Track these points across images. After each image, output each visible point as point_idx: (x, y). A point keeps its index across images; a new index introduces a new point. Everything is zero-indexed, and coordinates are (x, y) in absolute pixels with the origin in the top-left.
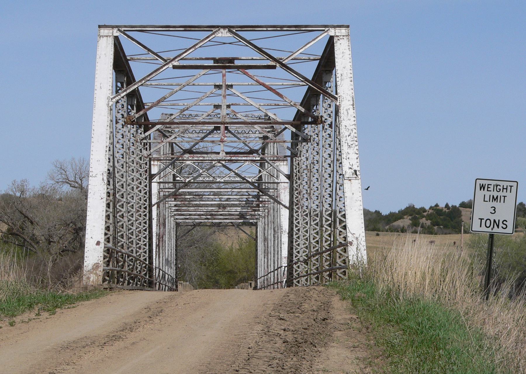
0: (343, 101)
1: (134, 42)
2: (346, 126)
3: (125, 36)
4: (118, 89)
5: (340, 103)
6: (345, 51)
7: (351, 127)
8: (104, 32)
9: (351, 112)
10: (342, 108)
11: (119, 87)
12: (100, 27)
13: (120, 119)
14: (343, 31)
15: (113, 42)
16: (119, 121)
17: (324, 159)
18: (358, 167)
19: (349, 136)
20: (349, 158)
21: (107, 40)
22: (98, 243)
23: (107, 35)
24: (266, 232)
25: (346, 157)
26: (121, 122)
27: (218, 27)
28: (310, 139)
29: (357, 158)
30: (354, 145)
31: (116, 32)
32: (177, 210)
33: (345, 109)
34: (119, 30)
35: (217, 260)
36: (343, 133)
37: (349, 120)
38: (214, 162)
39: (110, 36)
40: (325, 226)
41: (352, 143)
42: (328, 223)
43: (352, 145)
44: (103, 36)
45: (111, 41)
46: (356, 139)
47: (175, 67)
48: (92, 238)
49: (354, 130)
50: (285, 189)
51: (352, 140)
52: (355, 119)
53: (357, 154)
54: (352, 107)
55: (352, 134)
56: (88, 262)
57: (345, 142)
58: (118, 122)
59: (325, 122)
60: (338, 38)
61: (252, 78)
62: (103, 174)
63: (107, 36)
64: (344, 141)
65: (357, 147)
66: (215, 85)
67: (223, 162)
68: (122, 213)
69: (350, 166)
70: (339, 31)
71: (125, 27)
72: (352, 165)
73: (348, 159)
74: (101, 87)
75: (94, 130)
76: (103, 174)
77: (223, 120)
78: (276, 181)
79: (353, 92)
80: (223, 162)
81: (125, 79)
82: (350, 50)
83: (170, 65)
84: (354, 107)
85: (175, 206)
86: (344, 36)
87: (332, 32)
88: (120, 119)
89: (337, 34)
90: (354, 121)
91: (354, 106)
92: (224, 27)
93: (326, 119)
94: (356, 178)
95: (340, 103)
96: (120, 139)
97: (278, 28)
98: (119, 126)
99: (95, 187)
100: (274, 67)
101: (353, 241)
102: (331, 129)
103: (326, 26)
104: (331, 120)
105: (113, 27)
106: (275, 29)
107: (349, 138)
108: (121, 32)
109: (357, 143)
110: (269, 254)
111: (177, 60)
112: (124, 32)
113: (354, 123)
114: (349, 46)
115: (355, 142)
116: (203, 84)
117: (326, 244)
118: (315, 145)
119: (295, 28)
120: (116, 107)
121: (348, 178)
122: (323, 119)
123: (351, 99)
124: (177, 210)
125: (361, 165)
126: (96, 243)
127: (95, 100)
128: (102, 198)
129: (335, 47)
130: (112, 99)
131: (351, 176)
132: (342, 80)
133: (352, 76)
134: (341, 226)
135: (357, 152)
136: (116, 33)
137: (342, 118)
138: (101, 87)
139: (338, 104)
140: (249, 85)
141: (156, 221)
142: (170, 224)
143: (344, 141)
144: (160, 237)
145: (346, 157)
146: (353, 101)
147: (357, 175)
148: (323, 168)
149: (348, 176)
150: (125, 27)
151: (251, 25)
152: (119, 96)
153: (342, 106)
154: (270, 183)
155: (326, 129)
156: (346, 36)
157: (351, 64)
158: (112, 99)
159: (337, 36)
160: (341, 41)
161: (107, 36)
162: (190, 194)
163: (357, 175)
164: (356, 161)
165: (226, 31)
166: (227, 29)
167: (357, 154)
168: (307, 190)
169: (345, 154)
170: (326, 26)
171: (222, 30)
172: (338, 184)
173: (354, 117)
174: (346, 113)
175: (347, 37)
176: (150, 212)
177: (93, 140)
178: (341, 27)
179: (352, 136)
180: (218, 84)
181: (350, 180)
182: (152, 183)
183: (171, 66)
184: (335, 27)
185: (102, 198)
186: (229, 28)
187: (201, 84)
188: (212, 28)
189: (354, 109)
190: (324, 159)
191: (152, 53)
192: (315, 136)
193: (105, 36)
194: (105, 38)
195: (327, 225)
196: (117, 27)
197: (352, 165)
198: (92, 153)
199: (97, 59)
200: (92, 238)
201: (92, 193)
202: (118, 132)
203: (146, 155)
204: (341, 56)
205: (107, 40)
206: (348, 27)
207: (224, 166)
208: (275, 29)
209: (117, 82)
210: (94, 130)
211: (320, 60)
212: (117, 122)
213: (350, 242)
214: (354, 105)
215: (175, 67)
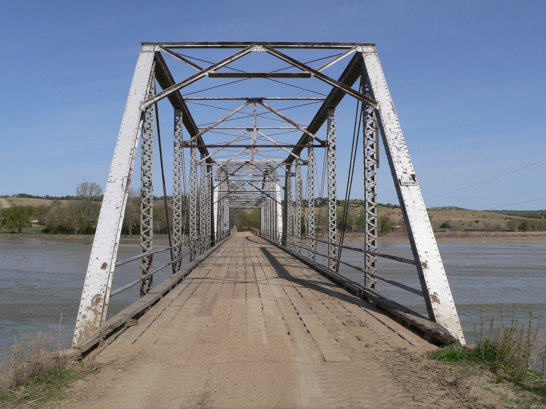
0: (382, 106)
1: (173, 56)
2: (391, 129)
3: (165, 51)
4: (176, 121)
5: (379, 107)
6: (374, 64)
7: (396, 130)
8: (146, 48)
9: (393, 115)
10: (382, 112)
11: (177, 120)
12: (143, 44)
13: (177, 144)
14: (370, 49)
15: (154, 56)
16: (177, 145)
17: (329, 173)
18: (413, 171)
19: (396, 139)
20: (400, 162)
21: (148, 54)
22: (104, 266)
23: (149, 50)
24: (266, 212)
25: (397, 160)
26: (178, 146)
27: (253, 43)
28: (308, 163)
29: (410, 162)
30: (403, 149)
31: (158, 48)
32: (229, 203)
33: (386, 113)
34: (160, 47)
35: (245, 217)
36: (389, 136)
37: (393, 123)
38: (245, 182)
39: (152, 51)
40: (331, 223)
41: (401, 146)
42: (333, 221)
43: (401, 148)
44: (144, 52)
45: (152, 56)
46: (404, 142)
47: (211, 75)
48: (97, 258)
49: (399, 133)
50: (279, 194)
51: (400, 143)
52: (398, 123)
53: (409, 158)
54: (392, 111)
55: (399, 137)
56: (87, 293)
57: (393, 146)
58: (176, 146)
59: (330, 146)
60: (366, 54)
61: (275, 113)
62: (123, 179)
63: (148, 52)
64: (392, 144)
65: (407, 151)
66: (247, 129)
67: (249, 182)
68: (178, 213)
69: (404, 171)
70: (366, 48)
71: (166, 43)
72: (406, 169)
73: (400, 163)
74: (135, 93)
75: (121, 133)
76: (123, 179)
77: (254, 144)
78: (275, 191)
79: (391, 98)
80: (249, 182)
81: (182, 114)
82: (379, 63)
83: (206, 74)
84: (394, 112)
85: (229, 201)
86: (371, 52)
87: (359, 49)
88: (177, 144)
89: (365, 51)
90: (398, 124)
91: (395, 111)
92: (259, 44)
93: (330, 143)
94: (414, 183)
95: (379, 107)
96: (177, 158)
97: (309, 45)
98: (177, 148)
99: (111, 194)
100: (308, 76)
101: (426, 261)
102: (334, 151)
103: (353, 44)
104: (334, 144)
105: (155, 44)
106: (306, 46)
107: (396, 141)
108: (162, 48)
109: (406, 147)
110: (268, 222)
111: (213, 69)
112: (165, 48)
113: (398, 126)
114: (377, 60)
115: (404, 145)
116: (240, 128)
117: (331, 236)
118: (311, 167)
119: (325, 45)
120: (174, 134)
121: (405, 183)
122: (329, 143)
123: (390, 104)
124: (229, 203)
125: (415, 167)
126: (101, 265)
127: (127, 105)
128: (117, 208)
129: (365, 61)
130: (144, 103)
131: (408, 181)
132: (377, 87)
133: (386, 84)
134: (370, 231)
135: (408, 156)
136: (157, 49)
137: (384, 121)
138: (135, 93)
139: (378, 108)
140: (268, 128)
141: (82, 302)
142: (227, 209)
143: (392, 144)
144: (220, 217)
145: (397, 160)
146: (392, 106)
147: (415, 181)
148: (329, 180)
149: (405, 182)
150: (166, 43)
151: (284, 41)
152: (152, 101)
153: (382, 110)
154: (270, 191)
155: (331, 151)
156: (373, 52)
157: (383, 74)
158: (144, 103)
159: (365, 52)
160: (369, 56)
161: (148, 52)
162: (234, 196)
163: (415, 181)
164: (409, 165)
165: (260, 47)
166: (262, 46)
167: (409, 158)
168: (299, 196)
169: (395, 157)
170: (353, 44)
171: (257, 46)
172: (367, 191)
173: (397, 120)
174: (388, 117)
175: (374, 53)
176: (212, 207)
177: (118, 143)
178: (367, 46)
179: (399, 139)
180: (249, 128)
181: (407, 186)
182: (214, 192)
183: (208, 74)
184: (361, 45)
185: (117, 208)
186: (264, 44)
187: (238, 128)
188: (247, 45)
189: (395, 114)
190: (329, 173)
191: (189, 64)
192: (311, 161)
193: (146, 51)
194: (146, 53)
195: (332, 222)
196: (158, 44)
197: (406, 169)
198: (115, 156)
199: (136, 70)
200: (97, 258)
201: (108, 201)
202: (176, 153)
203: (207, 175)
204: (372, 67)
205: (148, 54)
206: (374, 45)
207: (249, 183)
208: (306, 46)
209: (175, 116)
210: (121, 133)
211: (326, 100)
212: (175, 146)
213: (423, 263)
214: (394, 110)
215: (211, 75)
